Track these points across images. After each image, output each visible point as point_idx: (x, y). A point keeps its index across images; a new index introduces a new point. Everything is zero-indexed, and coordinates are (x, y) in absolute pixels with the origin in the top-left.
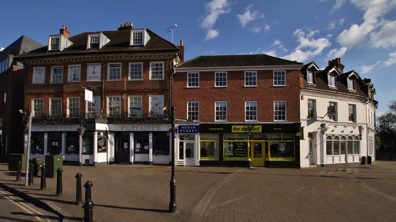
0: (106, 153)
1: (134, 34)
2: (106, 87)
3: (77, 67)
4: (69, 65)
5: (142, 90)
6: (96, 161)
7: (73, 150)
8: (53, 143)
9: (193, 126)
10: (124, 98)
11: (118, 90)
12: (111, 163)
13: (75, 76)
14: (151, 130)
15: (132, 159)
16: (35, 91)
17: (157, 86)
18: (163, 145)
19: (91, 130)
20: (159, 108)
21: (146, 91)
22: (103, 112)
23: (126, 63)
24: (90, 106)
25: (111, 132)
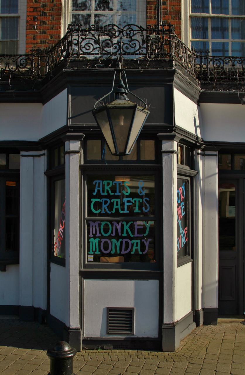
25: (210, 147)
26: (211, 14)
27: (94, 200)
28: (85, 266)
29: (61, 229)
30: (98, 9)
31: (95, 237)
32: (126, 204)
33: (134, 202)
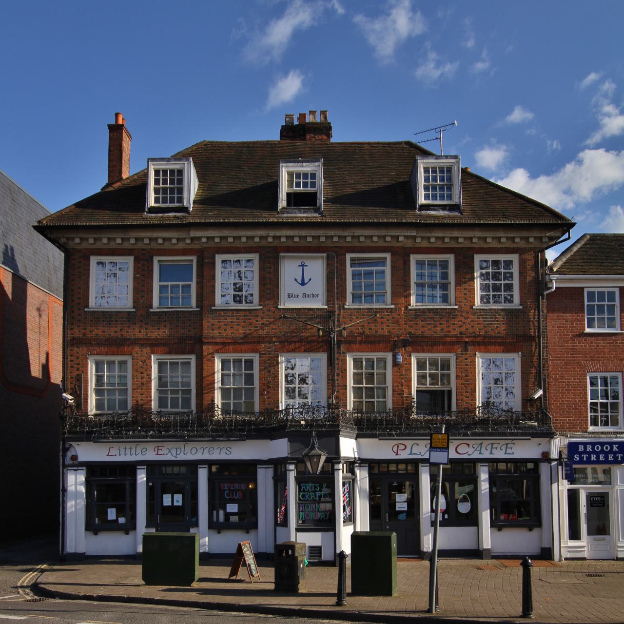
1: (426, 170)
3: (243, 263)
4: (217, 256)
5: (456, 336)
7: (234, 519)
8: (167, 500)
9: (611, 444)
11: (383, 336)
13: (240, 290)
14: (486, 455)
15: (427, 544)
16: (98, 332)
17: (500, 328)
18: (518, 501)
20: (506, 390)
21: (467, 340)
23: (401, 257)
24: (292, 382)
26: (364, 385)
27: (301, 493)
28: (298, 526)
29: (283, 508)
31: (302, 512)
32: (317, 495)
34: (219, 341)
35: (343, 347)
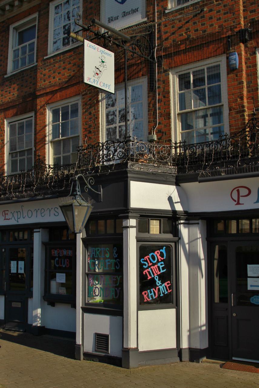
0: (173, 311)
2: (164, 37)
6: (132, 345)
10: (240, 63)
11: (212, 35)
12: (195, 355)
19: (113, 213)
22: (159, 139)
25: (191, 218)
28: (86, 304)
30: (121, 121)
32: (107, 263)
33: (111, 262)
34: (48, 91)
35: (164, 62)
